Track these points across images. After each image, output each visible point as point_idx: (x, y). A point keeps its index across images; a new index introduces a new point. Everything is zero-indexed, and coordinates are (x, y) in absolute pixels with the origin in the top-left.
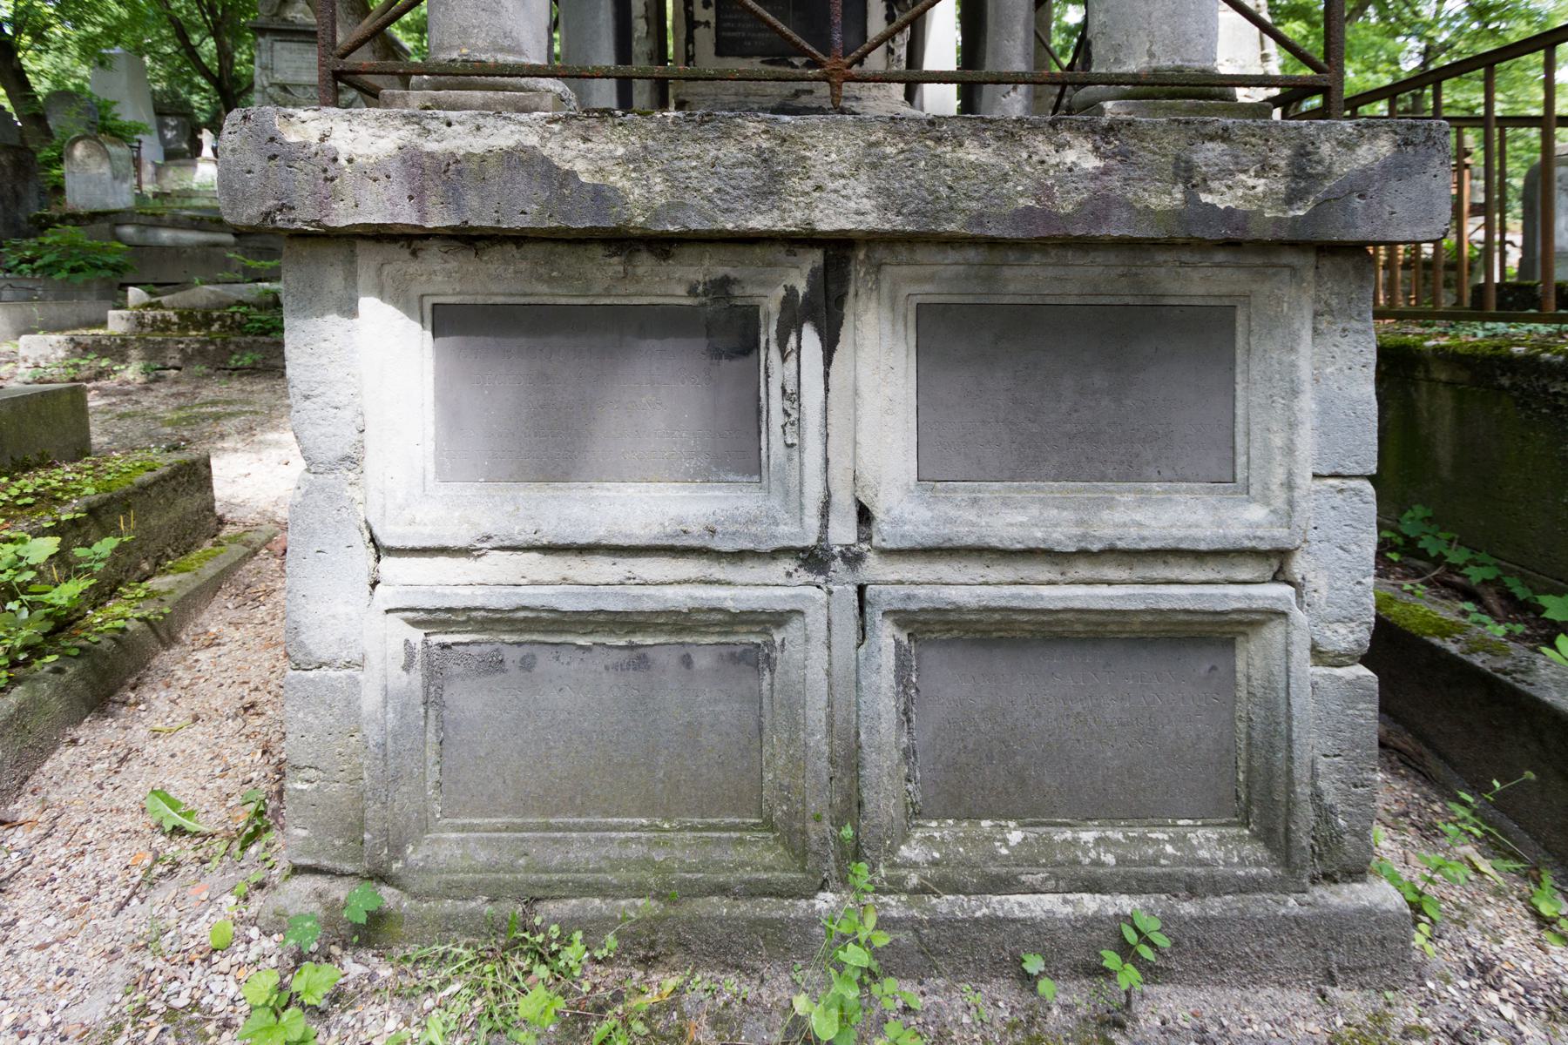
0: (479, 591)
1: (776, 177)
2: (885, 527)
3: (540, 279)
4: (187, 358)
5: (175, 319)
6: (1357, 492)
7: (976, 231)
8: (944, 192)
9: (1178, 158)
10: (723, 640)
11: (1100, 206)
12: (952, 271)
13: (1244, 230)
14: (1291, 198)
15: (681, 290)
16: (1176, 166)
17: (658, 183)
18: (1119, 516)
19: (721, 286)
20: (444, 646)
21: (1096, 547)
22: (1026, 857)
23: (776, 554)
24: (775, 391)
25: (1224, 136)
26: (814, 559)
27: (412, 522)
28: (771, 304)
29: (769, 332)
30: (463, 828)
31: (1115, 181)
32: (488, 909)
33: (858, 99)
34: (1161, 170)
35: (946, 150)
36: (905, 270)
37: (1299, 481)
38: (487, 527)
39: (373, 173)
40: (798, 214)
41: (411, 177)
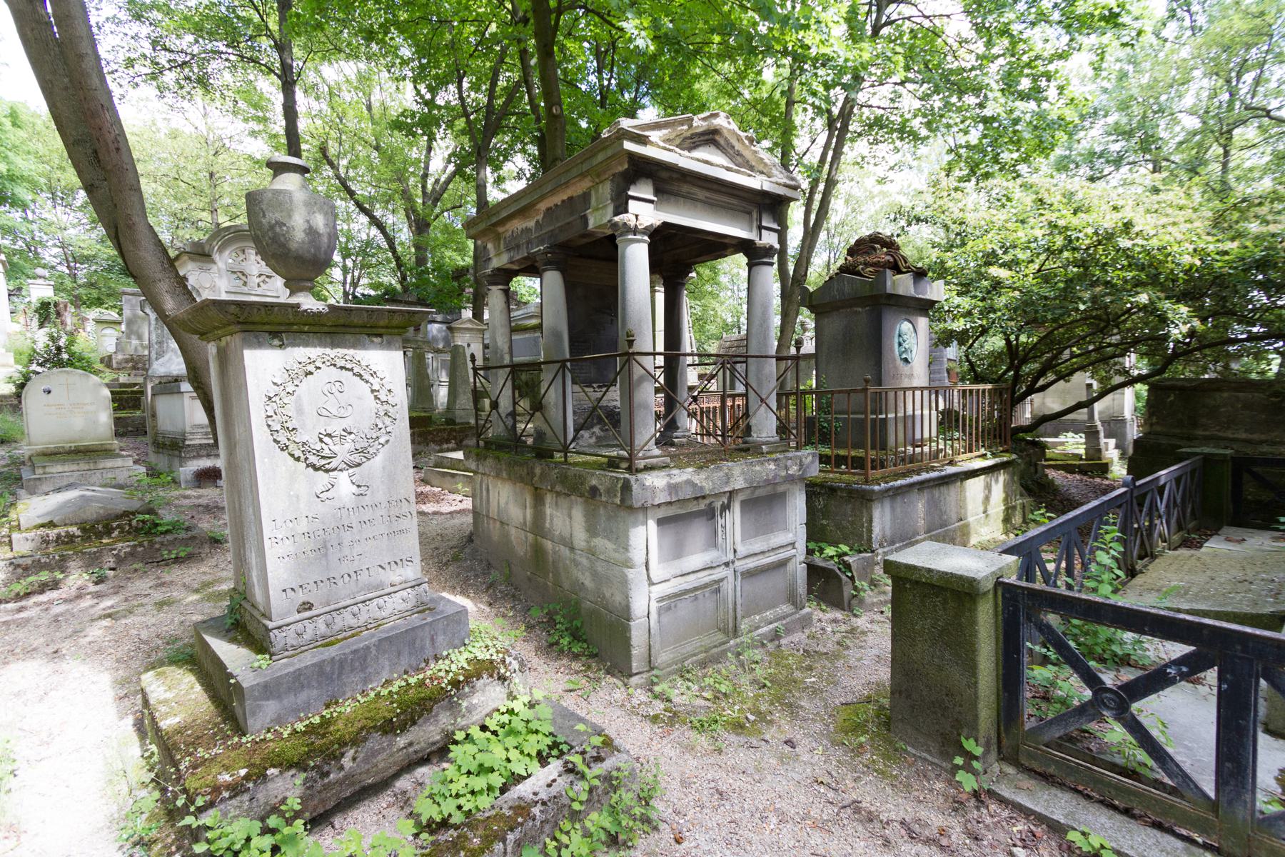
4: (120, 560)
5: (78, 533)
22: (760, 621)
26: (727, 564)
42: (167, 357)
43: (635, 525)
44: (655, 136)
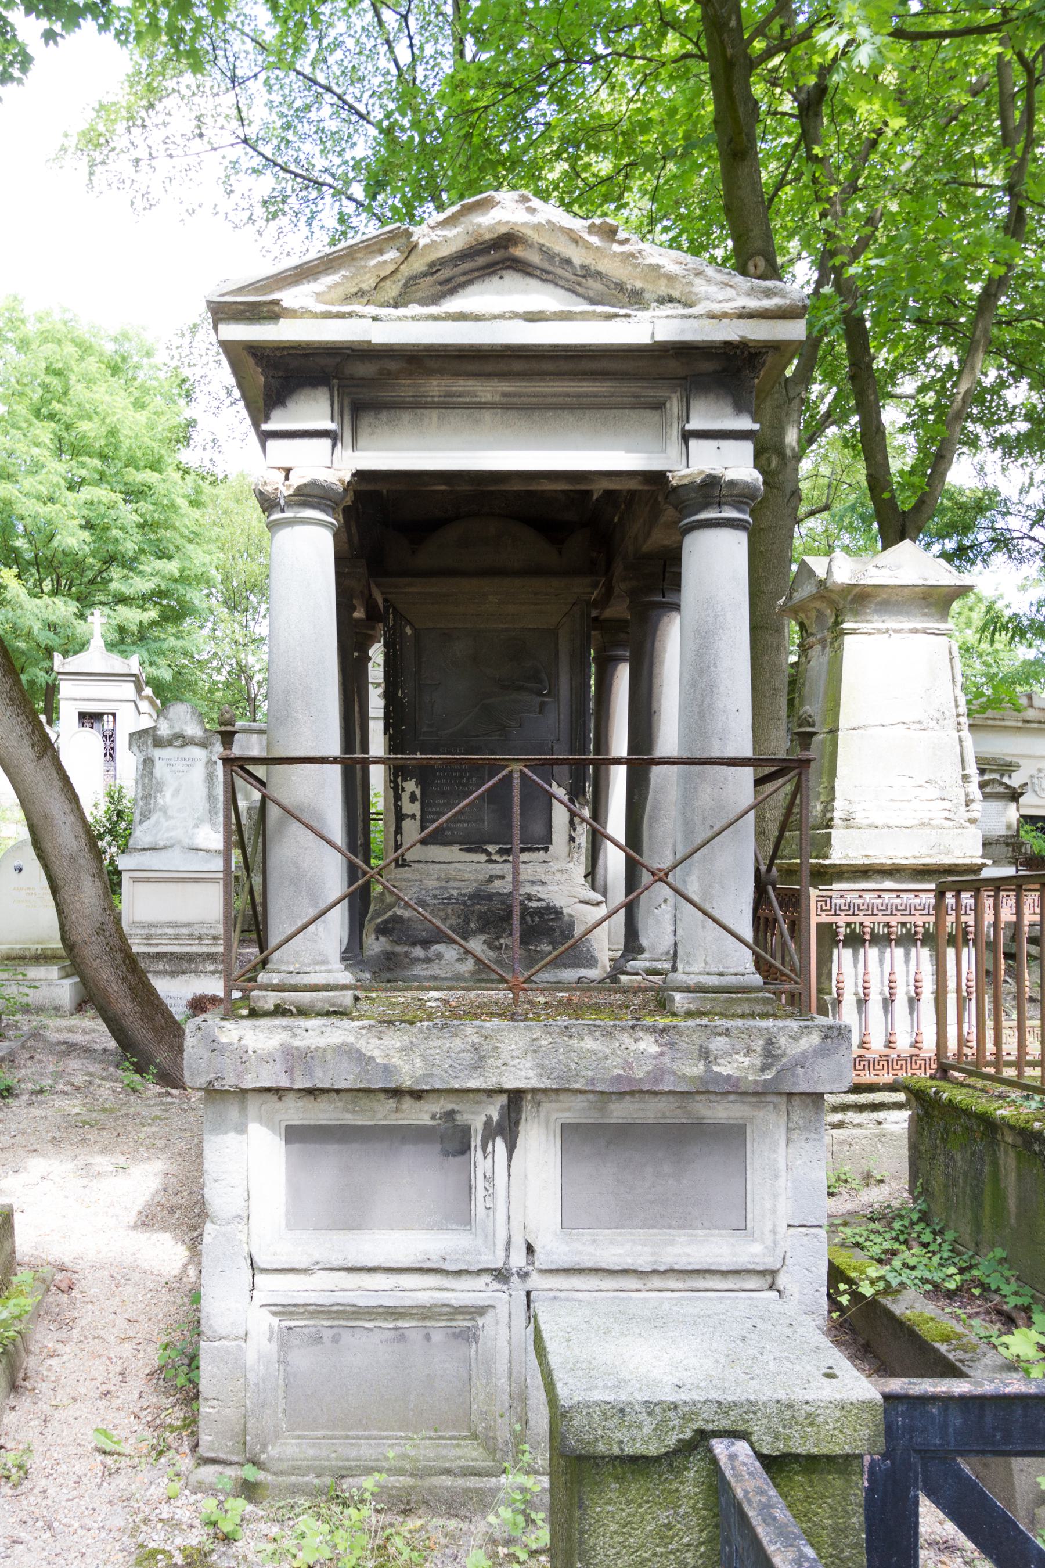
0: (313, 1294)
1: (482, 1058)
2: (542, 1257)
3: (348, 1111)
6: (816, 1236)
7: (590, 1088)
8: (573, 1066)
9: (701, 1046)
10: (449, 1324)
11: (658, 1074)
12: (580, 1106)
13: (738, 1087)
14: (764, 1069)
15: (427, 1117)
16: (700, 1051)
17: (418, 1062)
18: (676, 1250)
19: (450, 1115)
20: (290, 1328)
21: (662, 1268)
23: (480, 1272)
24: (480, 1176)
25: (727, 1033)
26: (501, 1275)
27: (275, 1254)
28: (478, 1125)
29: (476, 1141)
30: (299, 1437)
31: (666, 1059)
32: (316, 1481)
33: (543, 883)
34: (692, 1053)
35: (574, 1042)
36: (554, 1105)
37: (779, 1229)
38: (317, 1257)
39: (266, 1059)
40: (494, 1079)
41: (286, 1061)
42: (154, 818)
43: (219, 1128)
44: (290, 297)
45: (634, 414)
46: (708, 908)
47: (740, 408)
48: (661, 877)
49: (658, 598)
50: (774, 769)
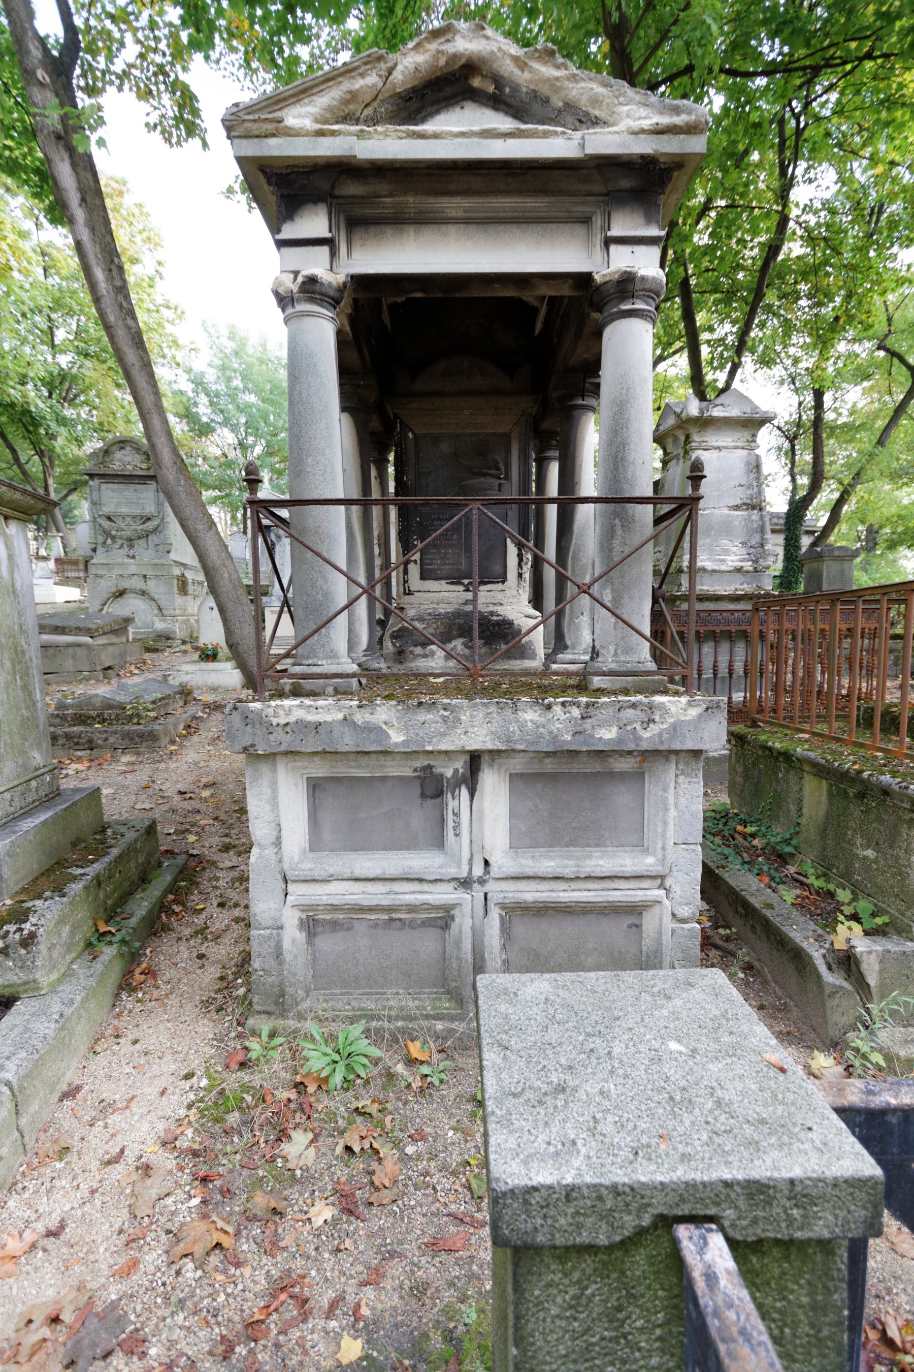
6: (694, 850)
18: (593, 862)
21: (582, 876)
26: (465, 883)
45: (567, 227)
46: (618, 612)
47: (649, 219)
48: (585, 589)
49: (581, 402)
50: (674, 506)
